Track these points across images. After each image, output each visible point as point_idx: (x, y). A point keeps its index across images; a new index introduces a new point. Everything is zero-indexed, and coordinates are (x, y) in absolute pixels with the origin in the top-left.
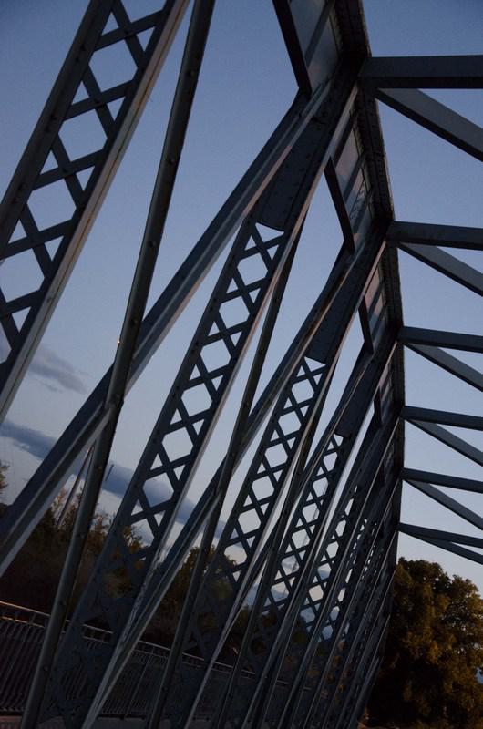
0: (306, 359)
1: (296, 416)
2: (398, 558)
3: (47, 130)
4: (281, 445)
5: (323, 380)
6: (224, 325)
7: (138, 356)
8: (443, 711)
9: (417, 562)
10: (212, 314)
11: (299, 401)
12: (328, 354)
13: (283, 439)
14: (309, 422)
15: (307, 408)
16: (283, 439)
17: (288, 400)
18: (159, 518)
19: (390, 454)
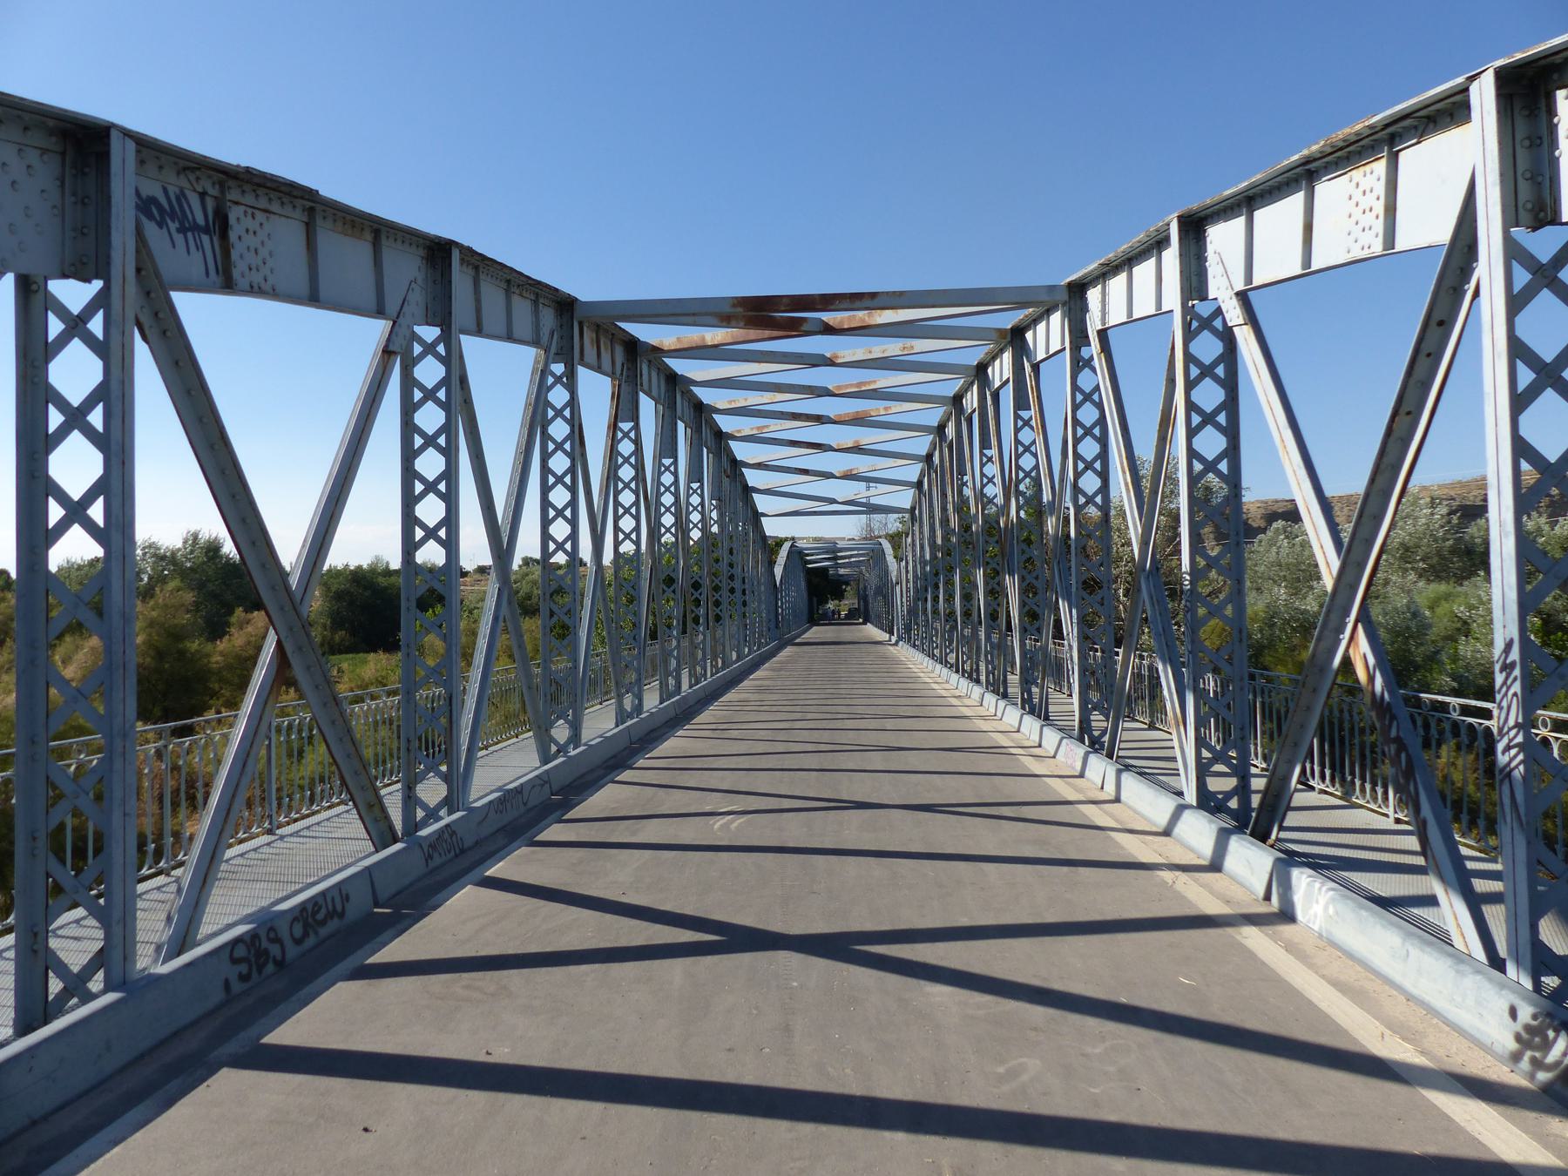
0: (984, 451)
1: (562, 388)
2: (733, 310)
3: (544, 500)
4: (559, 408)
5: (572, 413)
6: (1203, 363)
7: (675, 430)
8: (1534, 588)
9: (1087, 298)
10: (545, 504)
11: (430, 403)
12: (635, 417)
13: (430, 395)
14: (639, 468)
15: (99, 410)
16: (430, 395)
17: (51, 501)
18: (1198, 467)
19: (708, 431)
